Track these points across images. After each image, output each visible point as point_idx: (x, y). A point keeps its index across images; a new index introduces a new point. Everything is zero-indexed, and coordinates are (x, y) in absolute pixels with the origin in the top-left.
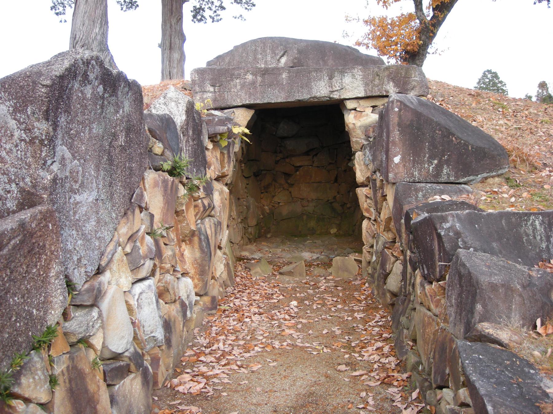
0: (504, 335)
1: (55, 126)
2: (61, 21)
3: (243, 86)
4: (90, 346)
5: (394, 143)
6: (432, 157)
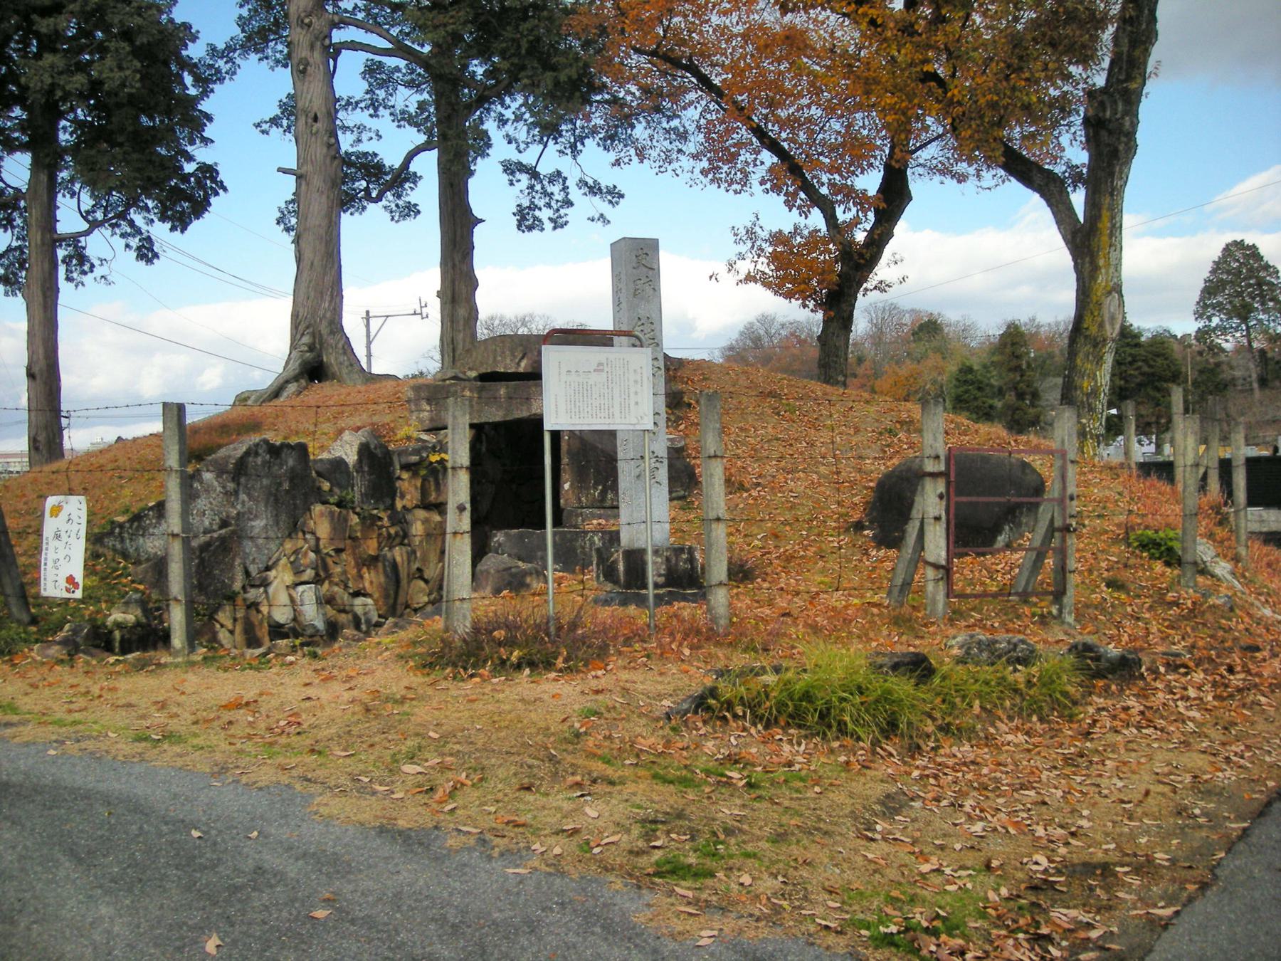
1: (238, 484)
4: (259, 611)
6: (596, 484)
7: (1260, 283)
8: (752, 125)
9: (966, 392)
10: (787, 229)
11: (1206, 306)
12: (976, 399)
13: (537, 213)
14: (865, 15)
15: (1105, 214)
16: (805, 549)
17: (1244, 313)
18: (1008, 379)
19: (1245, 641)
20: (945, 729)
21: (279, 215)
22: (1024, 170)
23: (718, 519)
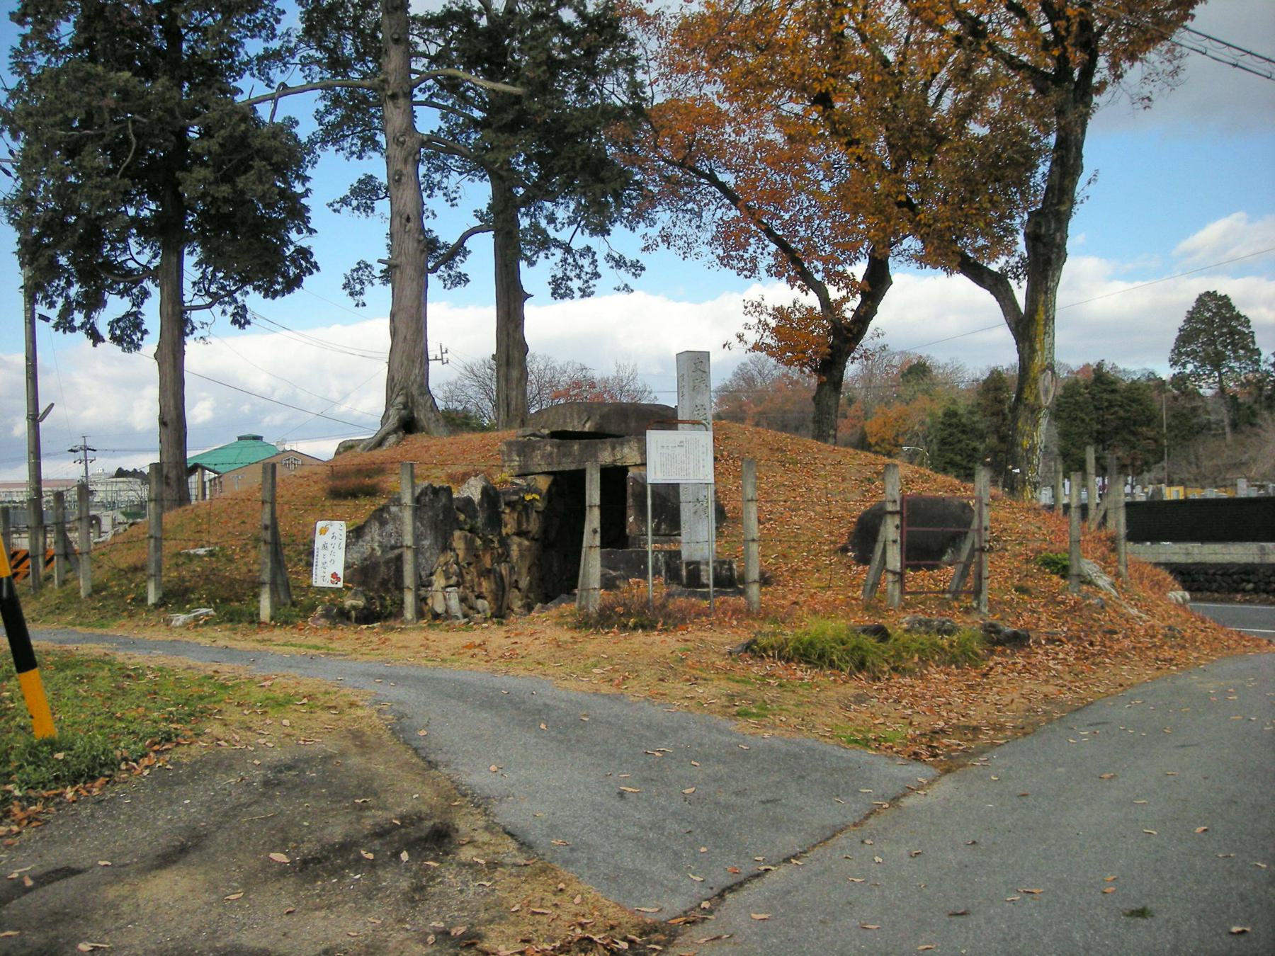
3: (543, 456)
7: (1232, 332)
8: (757, 227)
9: (951, 435)
10: (787, 303)
11: (1180, 354)
12: (960, 441)
13: (569, 283)
14: (853, 153)
15: (1041, 308)
16: (806, 564)
17: (1216, 361)
18: (980, 429)
19: (1109, 626)
20: (895, 669)
21: (344, 281)
22: (978, 274)
23: (753, 540)
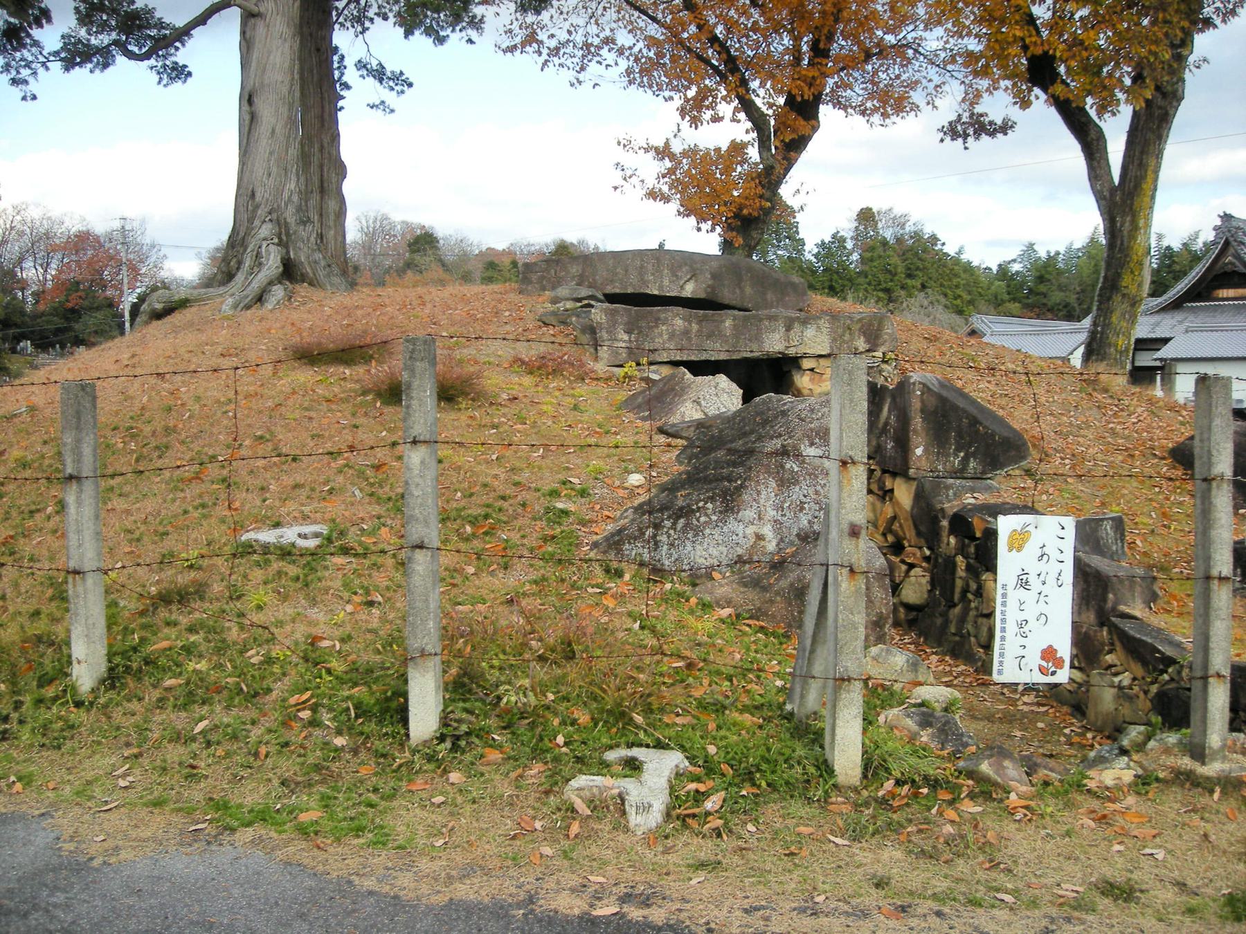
0: (1137, 613)
2: (24, 98)
3: (672, 336)
5: (915, 431)
6: (958, 450)
